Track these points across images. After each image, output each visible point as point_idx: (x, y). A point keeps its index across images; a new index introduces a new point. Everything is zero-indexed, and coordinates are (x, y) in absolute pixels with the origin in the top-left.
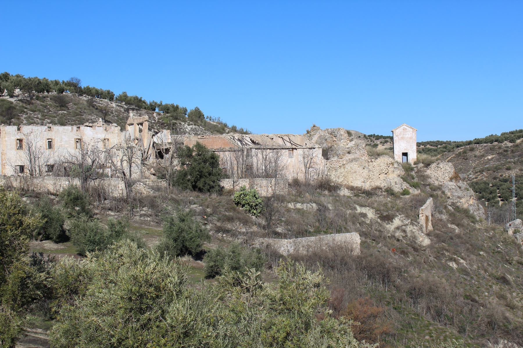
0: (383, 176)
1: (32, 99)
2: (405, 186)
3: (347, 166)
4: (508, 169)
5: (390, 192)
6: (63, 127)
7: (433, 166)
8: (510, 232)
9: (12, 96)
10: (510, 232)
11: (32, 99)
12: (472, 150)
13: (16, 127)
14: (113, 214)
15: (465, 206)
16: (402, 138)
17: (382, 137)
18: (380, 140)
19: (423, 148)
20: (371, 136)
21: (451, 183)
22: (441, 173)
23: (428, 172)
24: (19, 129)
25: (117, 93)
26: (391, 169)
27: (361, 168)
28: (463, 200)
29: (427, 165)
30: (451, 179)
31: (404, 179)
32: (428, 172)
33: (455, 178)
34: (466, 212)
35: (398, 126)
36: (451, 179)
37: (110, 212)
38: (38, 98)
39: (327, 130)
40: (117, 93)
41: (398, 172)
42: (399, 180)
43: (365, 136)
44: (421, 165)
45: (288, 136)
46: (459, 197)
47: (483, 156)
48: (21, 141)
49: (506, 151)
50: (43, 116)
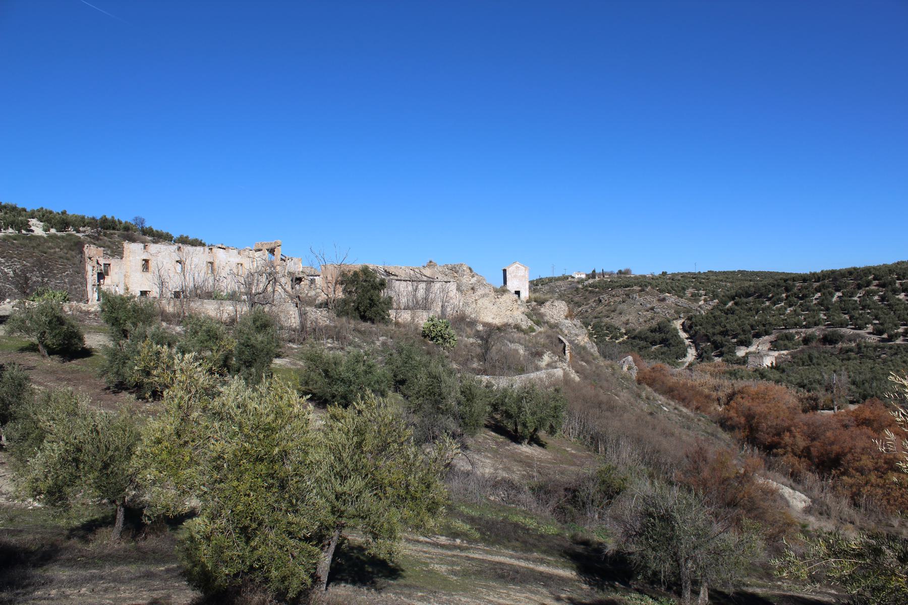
0: (509, 313)
1: (99, 235)
2: (530, 323)
3: (479, 302)
5: (518, 328)
6: (194, 248)
7: (548, 304)
8: (625, 369)
9: (78, 232)
10: (625, 369)
11: (99, 235)
13: (142, 245)
14: (295, 346)
15: (582, 343)
16: (515, 276)
19: (534, 285)
21: (567, 321)
22: (556, 311)
23: (543, 310)
24: (145, 247)
25: (176, 235)
26: (516, 306)
27: (491, 304)
28: (580, 338)
29: (541, 303)
30: (566, 318)
31: (529, 316)
32: (543, 310)
33: (569, 316)
34: (584, 348)
35: (510, 265)
36: (566, 318)
37: (291, 345)
38: (105, 235)
39: (447, 265)
40: (176, 235)
41: (522, 309)
42: (524, 317)
44: (534, 303)
45: (418, 268)
46: (577, 335)
48: (146, 261)
50: (112, 252)
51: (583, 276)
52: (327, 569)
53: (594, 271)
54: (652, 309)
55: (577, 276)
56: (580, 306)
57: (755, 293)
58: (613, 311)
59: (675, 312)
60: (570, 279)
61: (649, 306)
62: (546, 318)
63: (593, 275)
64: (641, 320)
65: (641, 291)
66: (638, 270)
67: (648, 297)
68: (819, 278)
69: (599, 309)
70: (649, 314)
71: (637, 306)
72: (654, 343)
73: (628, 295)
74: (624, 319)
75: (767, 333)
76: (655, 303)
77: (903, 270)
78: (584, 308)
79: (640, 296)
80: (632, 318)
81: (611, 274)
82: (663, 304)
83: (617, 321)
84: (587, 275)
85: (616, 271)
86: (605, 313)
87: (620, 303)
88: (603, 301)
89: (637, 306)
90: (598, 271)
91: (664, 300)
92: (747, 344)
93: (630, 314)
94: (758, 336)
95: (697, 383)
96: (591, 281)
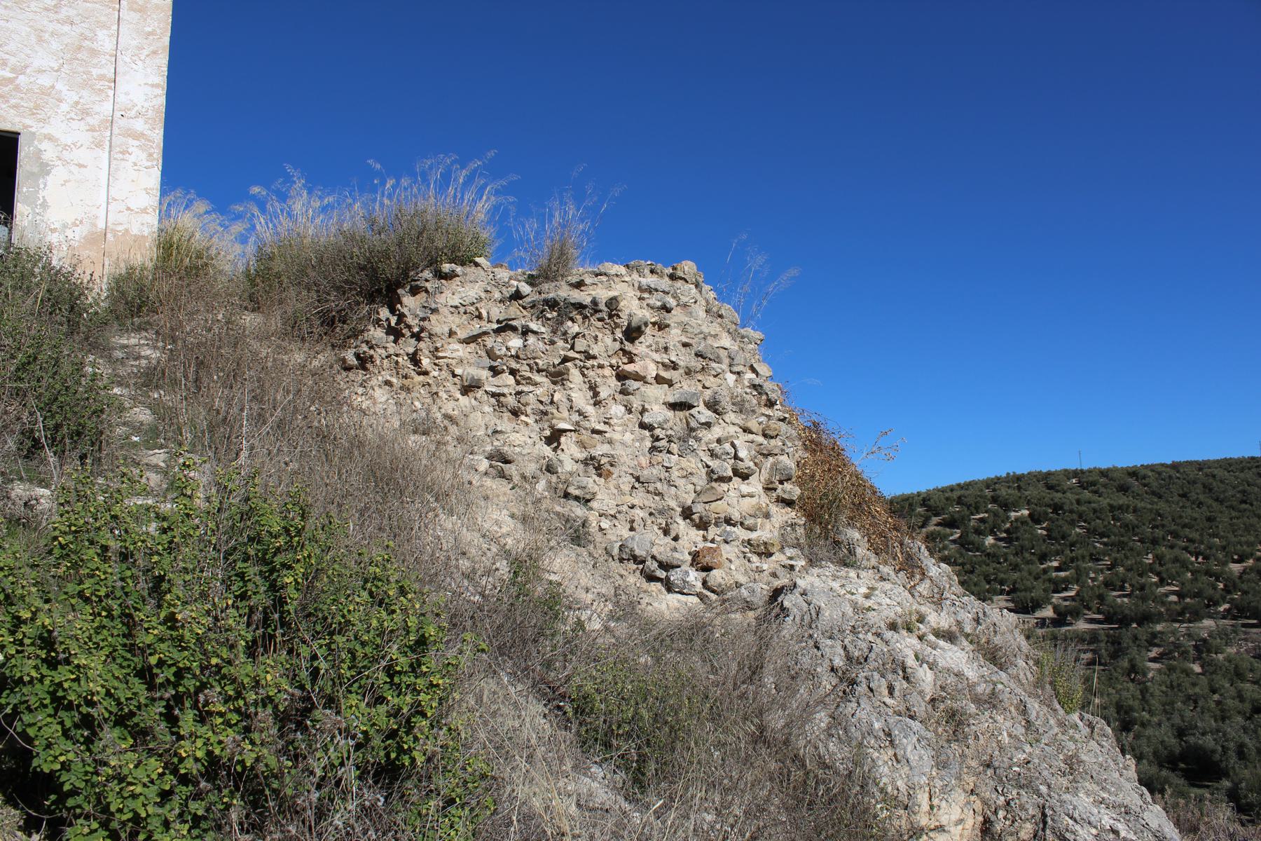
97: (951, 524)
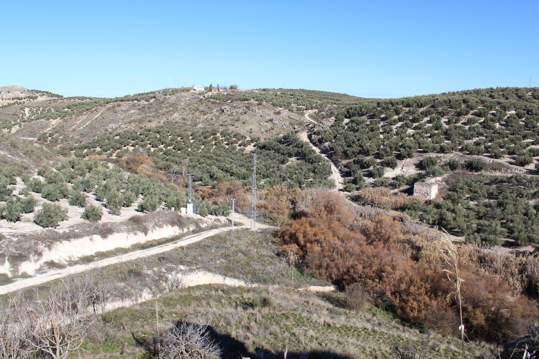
4: (150, 121)
12: (119, 106)
17: (40, 91)
18: (39, 94)
20: (33, 90)
43: (28, 90)
47: (128, 110)
49: (144, 108)
51: (203, 89)
52: (263, 225)
53: (211, 86)
54: (271, 120)
55: (197, 89)
56: (205, 114)
57: (367, 113)
58: (237, 121)
59: (290, 123)
60: (192, 91)
61: (268, 118)
62: (64, 97)
63: (210, 89)
64: (263, 130)
65: (259, 105)
66: (244, 86)
67: (266, 110)
68: (422, 104)
69: (223, 117)
70: (269, 125)
71: (258, 117)
72: (290, 155)
73: (248, 108)
74: (248, 128)
75: (410, 156)
76: (272, 116)
77: (538, 94)
78: (209, 116)
79: (259, 109)
80: (255, 127)
81: (225, 89)
82: (279, 117)
83: (242, 130)
84: (206, 89)
85: (228, 86)
86: (230, 122)
87: (241, 113)
88: (225, 111)
89: (258, 117)
90: (215, 85)
91: (279, 113)
92: (392, 165)
93: (252, 124)
94: (400, 157)
95: (352, 301)
96: (210, 94)
97: (479, 115)
